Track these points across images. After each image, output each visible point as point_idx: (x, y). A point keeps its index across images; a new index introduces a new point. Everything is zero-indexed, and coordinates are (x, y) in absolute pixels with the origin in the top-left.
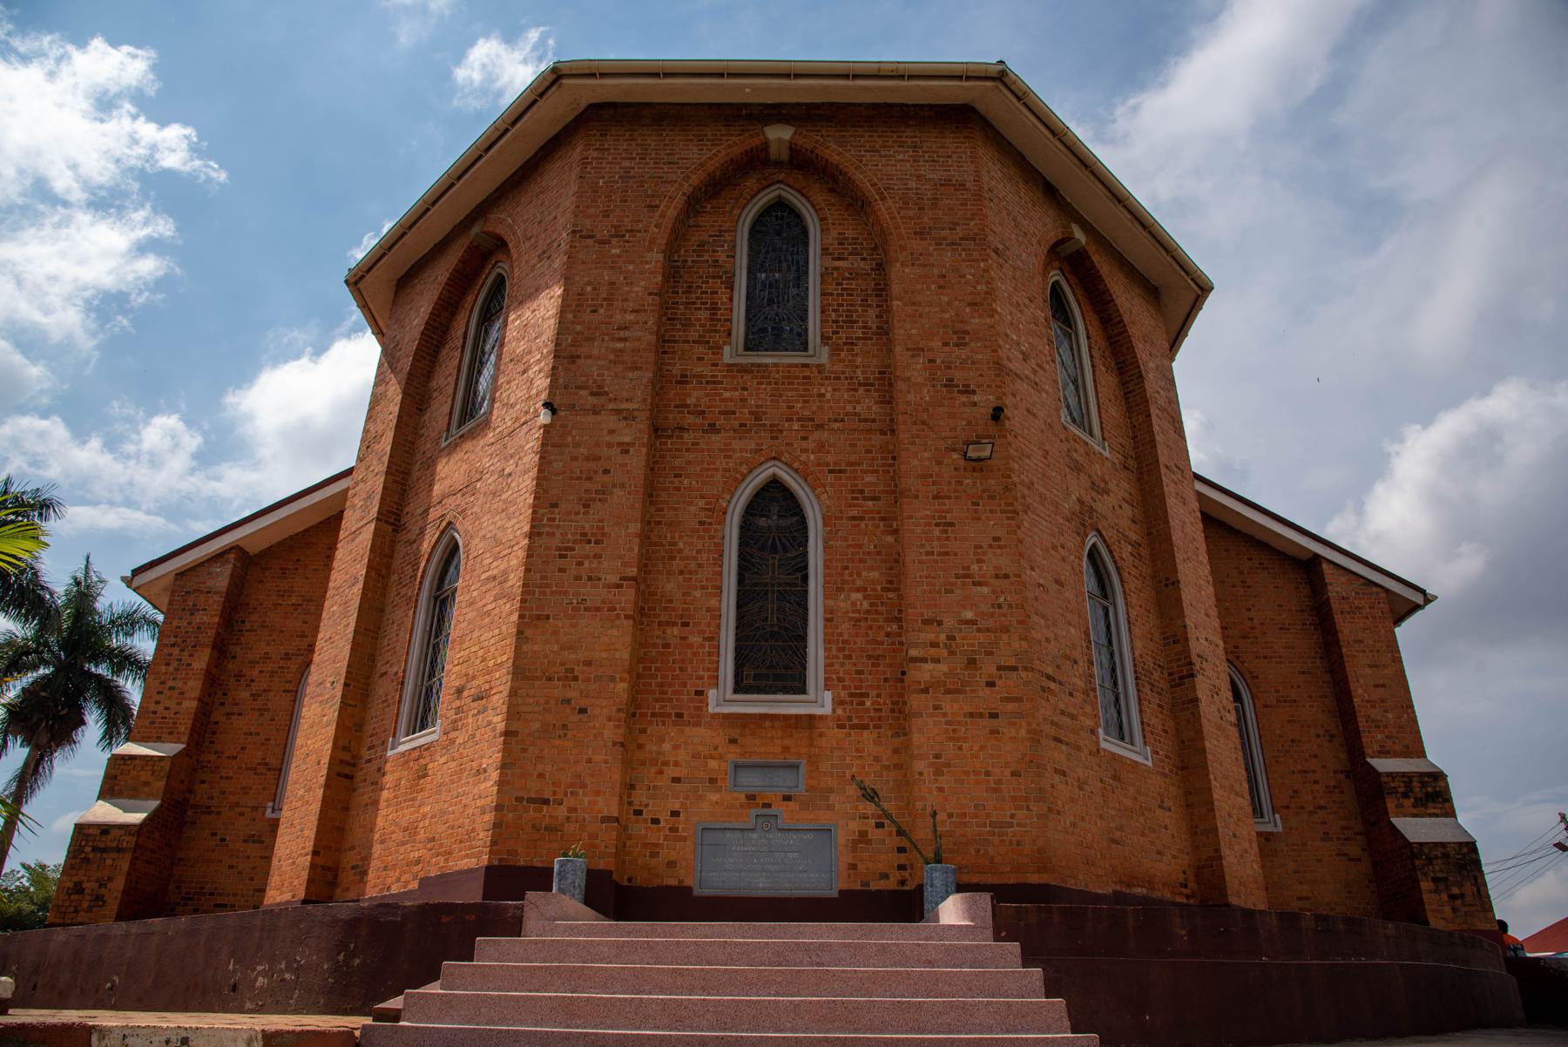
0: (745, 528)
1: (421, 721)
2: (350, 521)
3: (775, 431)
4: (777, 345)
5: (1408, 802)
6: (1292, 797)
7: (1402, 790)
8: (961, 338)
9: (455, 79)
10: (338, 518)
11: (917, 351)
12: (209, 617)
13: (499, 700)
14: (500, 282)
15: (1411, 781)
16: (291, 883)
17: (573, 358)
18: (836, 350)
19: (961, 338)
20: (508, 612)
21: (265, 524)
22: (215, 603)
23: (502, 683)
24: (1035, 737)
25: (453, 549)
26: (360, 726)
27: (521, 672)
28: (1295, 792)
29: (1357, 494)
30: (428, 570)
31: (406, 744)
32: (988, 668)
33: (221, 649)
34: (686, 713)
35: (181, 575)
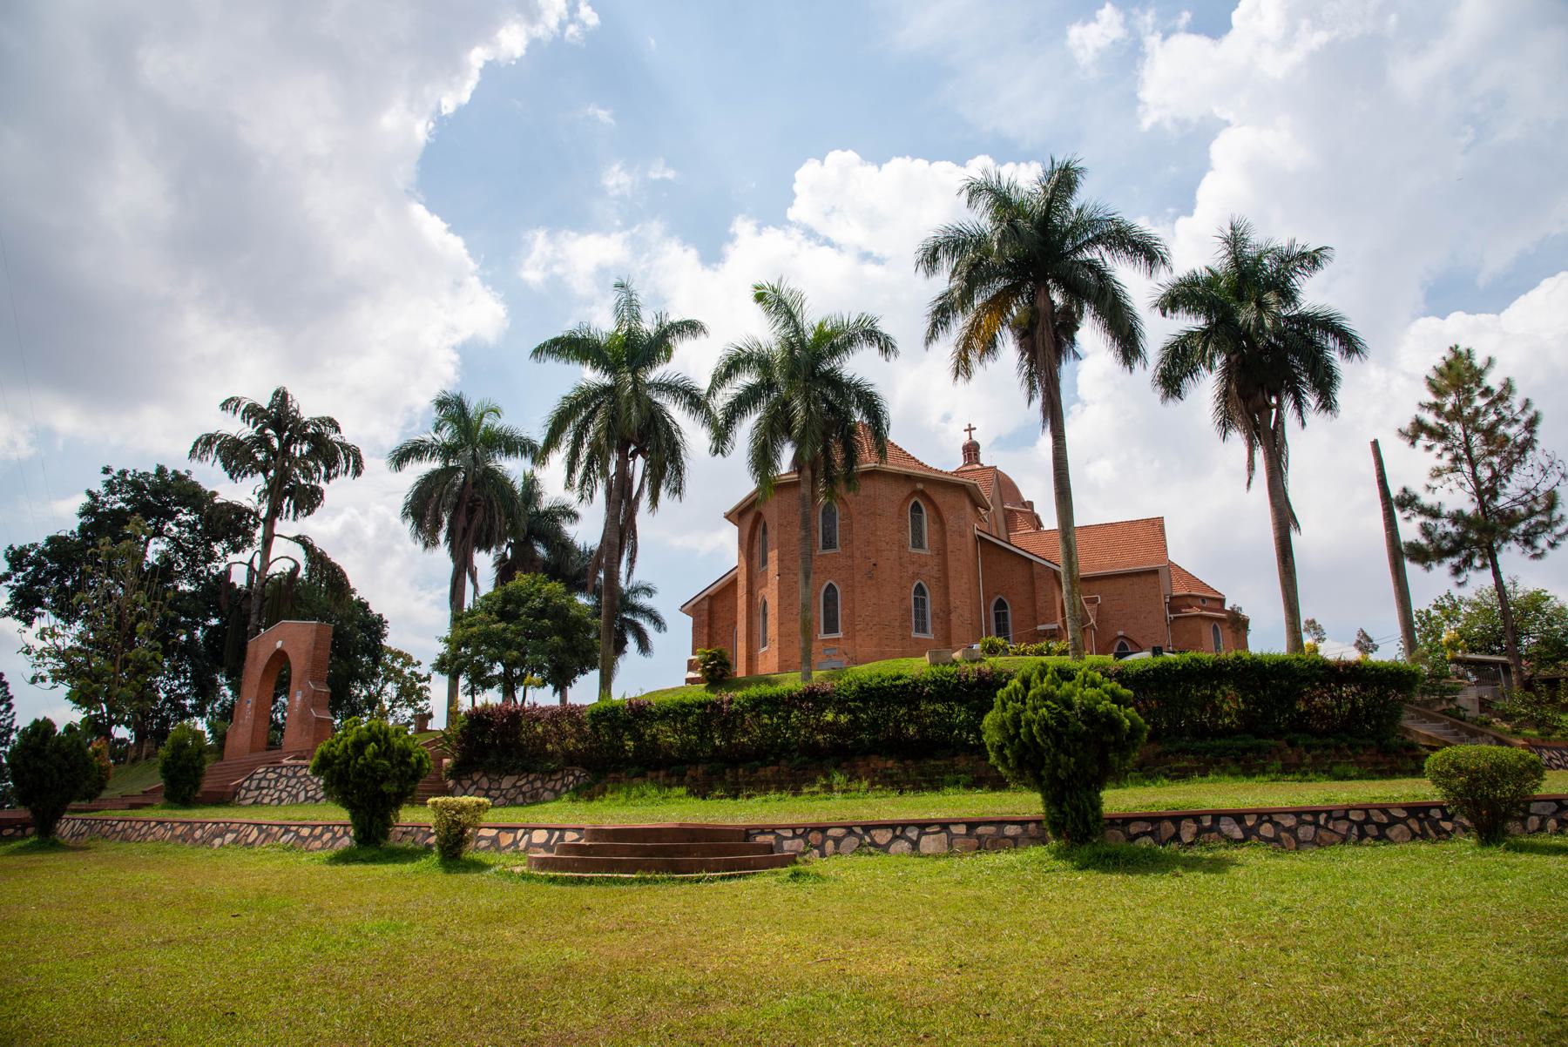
0: (825, 596)
1: (765, 645)
2: (739, 579)
3: (829, 572)
4: (830, 547)
8: (868, 543)
10: (736, 579)
11: (858, 549)
12: (705, 617)
13: (777, 641)
14: (765, 525)
17: (783, 561)
18: (843, 548)
19: (868, 543)
20: (776, 622)
22: (706, 612)
23: (777, 637)
24: (880, 639)
25: (765, 603)
26: (751, 647)
27: (780, 635)
30: (761, 607)
31: (763, 650)
32: (871, 625)
33: (710, 626)
35: (694, 606)
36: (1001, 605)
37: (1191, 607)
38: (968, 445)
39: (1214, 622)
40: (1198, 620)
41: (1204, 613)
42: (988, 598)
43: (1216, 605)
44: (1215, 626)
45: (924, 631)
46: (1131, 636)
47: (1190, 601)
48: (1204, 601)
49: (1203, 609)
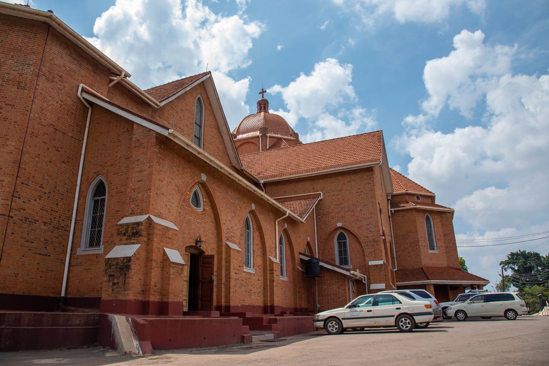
5: (124, 238)
6: (110, 237)
7: (123, 232)
9: (405, 118)
15: (128, 227)
16: (543, 271)
21: (144, 124)
28: (112, 235)
29: (457, 234)
34: (47, 197)
36: (100, 189)
37: (407, 202)
38: (261, 101)
39: (427, 214)
40: (414, 212)
41: (418, 206)
42: (86, 181)
43: (429, 201)
44: (427, 217)
45: (434, 249)
46: (349, 227)
47: (407, 198)
48: (418, 198)
49: (417, 203)
